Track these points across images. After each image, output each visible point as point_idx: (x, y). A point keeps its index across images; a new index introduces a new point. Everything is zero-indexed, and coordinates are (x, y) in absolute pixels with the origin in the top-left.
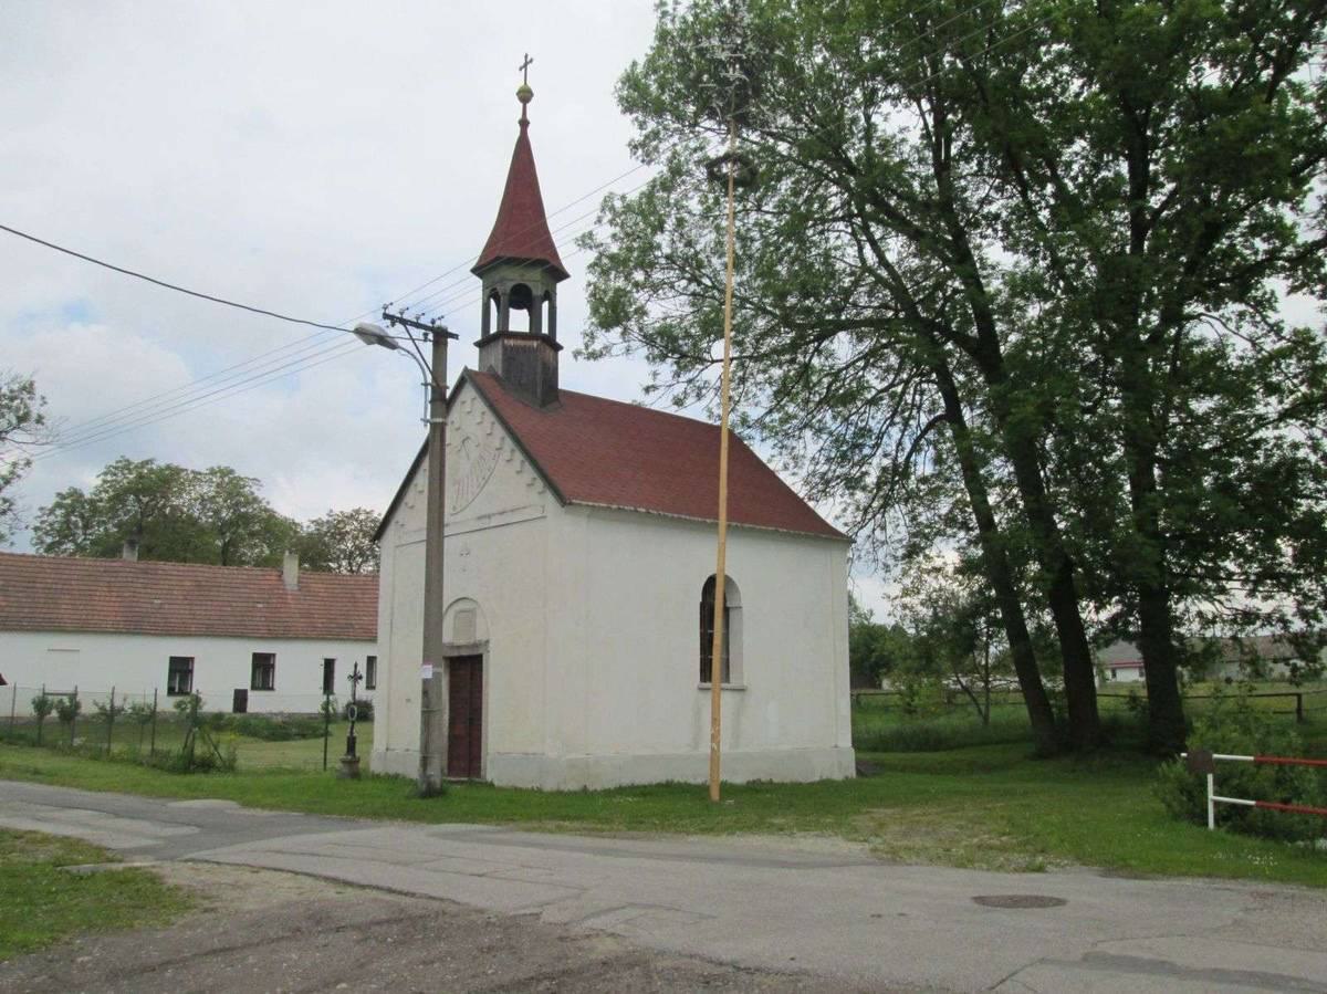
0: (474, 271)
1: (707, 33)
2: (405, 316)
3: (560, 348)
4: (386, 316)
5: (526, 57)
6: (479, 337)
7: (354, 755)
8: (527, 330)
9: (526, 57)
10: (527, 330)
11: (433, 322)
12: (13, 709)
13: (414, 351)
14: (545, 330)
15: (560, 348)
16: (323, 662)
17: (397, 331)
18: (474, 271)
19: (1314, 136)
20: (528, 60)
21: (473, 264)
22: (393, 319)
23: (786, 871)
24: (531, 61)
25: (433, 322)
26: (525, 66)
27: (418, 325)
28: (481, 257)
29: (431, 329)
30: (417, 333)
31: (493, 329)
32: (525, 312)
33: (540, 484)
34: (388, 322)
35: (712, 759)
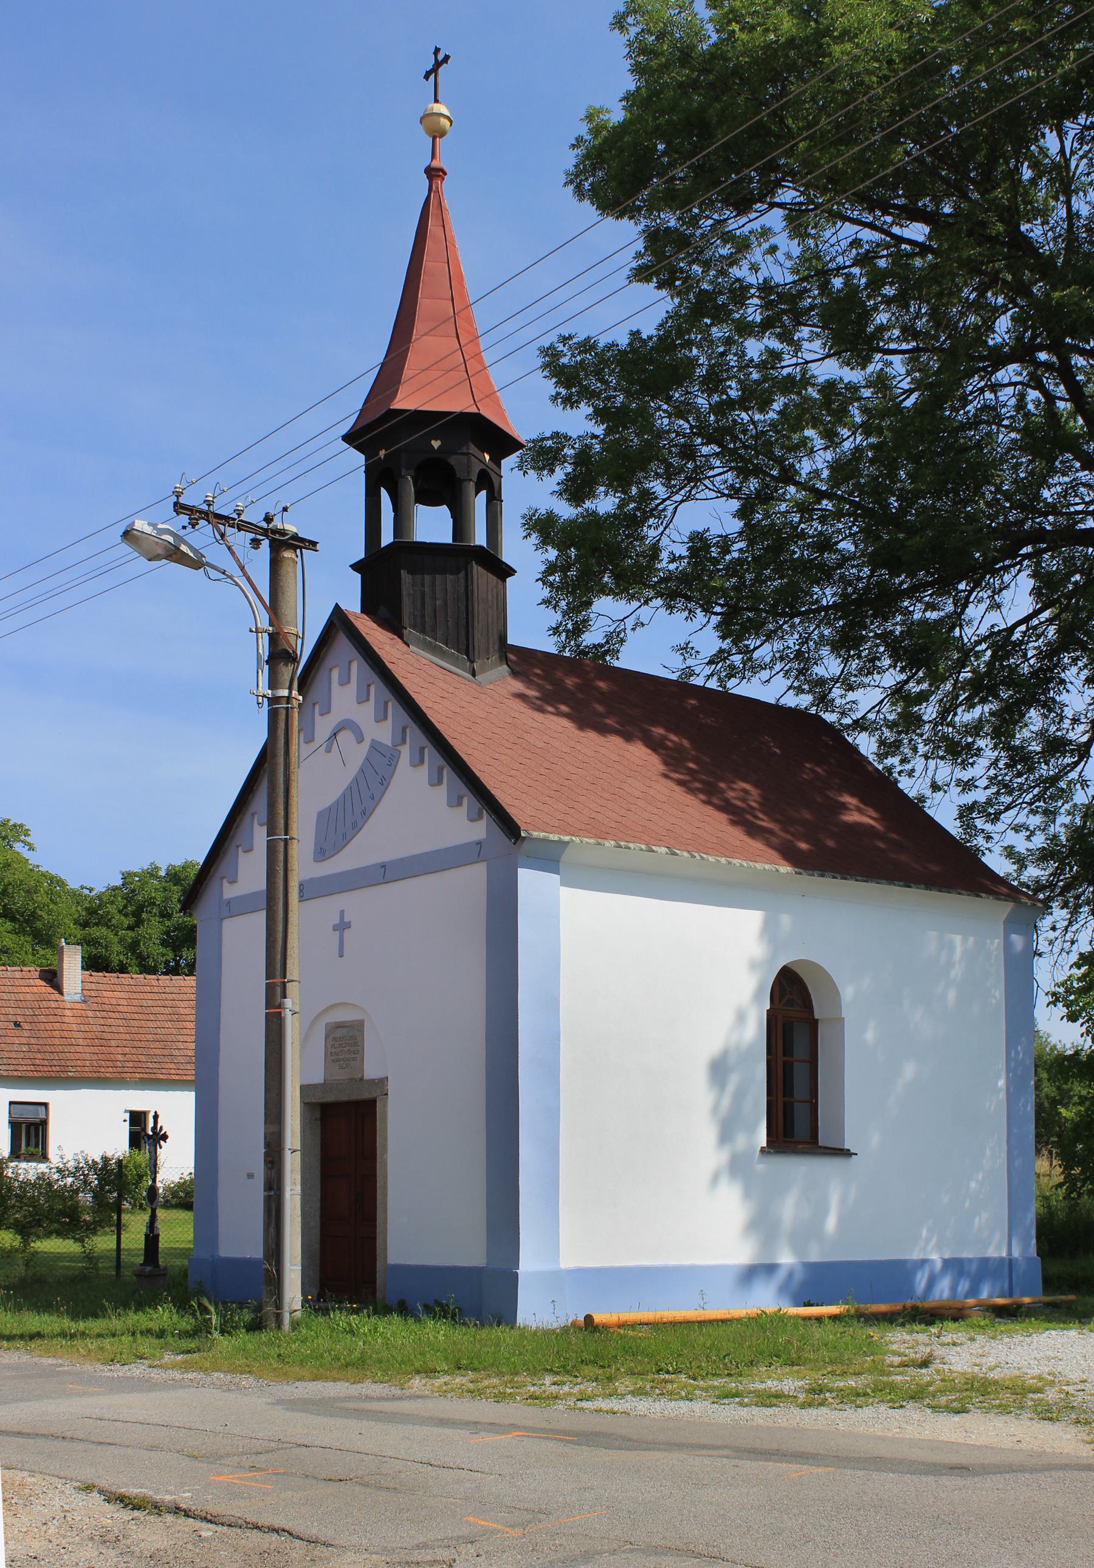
0: (349, 438)
1: (1042, 171)
2: (217, 508)
3: (508, 571)
4: (179, 508)
5: (437, 51)
6: (360, 554)
7: (157, 1265)
8: (449, 540)
9: (437, 51)
10: (449, 540)
11: (268, 519)
12: (803, 1061)
13: (236, 572)
14: (480, 538)
15: (508, 571)
16: (127, 1116)
17: (202, 537)
18: (349, 438)
19: (1083, 81)
20: (440, 57)
21: (346, 427)
22: (195, 515)
23: (448, 1431)
24: (446, 58)
25: (268, 519)
26: (435, 70)
27: (243, 526)
28: (362, 411)
29: (265, 532)
30: (240, 539)
31: (387, 537)
32: (444, 511)
33: (468, 799)
34: (184, 519)
35: (842, 1150)
